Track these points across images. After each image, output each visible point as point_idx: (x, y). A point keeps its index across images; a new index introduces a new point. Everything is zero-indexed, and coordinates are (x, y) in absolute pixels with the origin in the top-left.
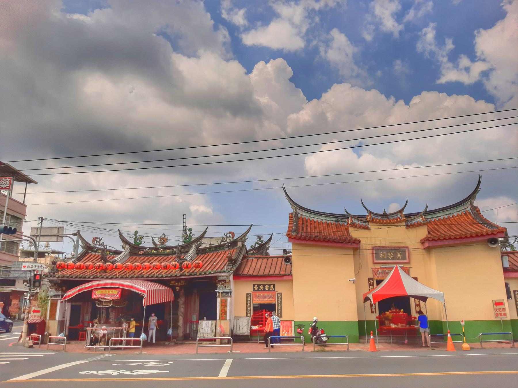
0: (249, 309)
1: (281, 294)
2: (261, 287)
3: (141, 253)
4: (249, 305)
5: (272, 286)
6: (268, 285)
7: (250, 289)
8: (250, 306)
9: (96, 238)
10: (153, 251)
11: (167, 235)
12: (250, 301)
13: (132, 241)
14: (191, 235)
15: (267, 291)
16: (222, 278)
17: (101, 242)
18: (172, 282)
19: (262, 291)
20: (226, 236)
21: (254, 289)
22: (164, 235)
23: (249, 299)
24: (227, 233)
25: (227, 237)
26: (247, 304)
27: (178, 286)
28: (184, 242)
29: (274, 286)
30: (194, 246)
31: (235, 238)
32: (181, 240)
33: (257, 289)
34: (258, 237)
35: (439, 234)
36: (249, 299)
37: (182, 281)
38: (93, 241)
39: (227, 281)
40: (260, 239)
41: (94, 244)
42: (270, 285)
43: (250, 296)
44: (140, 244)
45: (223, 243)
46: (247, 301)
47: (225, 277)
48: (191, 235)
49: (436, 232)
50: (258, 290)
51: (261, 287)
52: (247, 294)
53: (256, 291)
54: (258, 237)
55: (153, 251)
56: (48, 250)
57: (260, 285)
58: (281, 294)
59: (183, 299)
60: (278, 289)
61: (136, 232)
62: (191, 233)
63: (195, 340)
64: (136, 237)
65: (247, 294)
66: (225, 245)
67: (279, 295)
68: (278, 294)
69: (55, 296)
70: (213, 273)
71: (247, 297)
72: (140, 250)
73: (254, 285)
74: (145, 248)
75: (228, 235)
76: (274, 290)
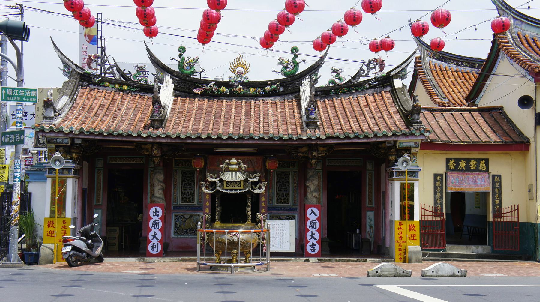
0: (439, 202)
1: (500, 176)
2: (463, 164)
4: (439, 194)
5: (482, 164)
6: (476, 160)
7: (441, 169)
8: (442, 197)
10: (223, 89)
11: (247, 59)
12: (441, 187)
13: (174, 66)
14: (298, 60)
15: (473, 170)
18: (305, 149)
19: (463, 170)
20: (368, 66)
21: (448, 167)
22: (241, 57)
23: (438, 184)
24: (370, 62)
25: (369, 68)
28: (284, 74)
29: (487, 161)
30: (307, 82)
31: (386, 70)
32: (280, 68)
33: (455, 166)
34: (335, 71)
36: (438, 184)
37: (321, 149)
39: (413, 151)
40: (338, 74)
42: (478, 161)
43: (441, 179)
45: (361, 79)
46: (435, 188)
47: (412, 144)
48: (298, 60)
50: (457, 169)
51: (463, 164)
52: (436, 175)
53: (453, 170)
54: (335, 71)
55: (223, 89)
57: (460, 160)
58: (500, 176)
59: (161, 177)
60: (494, 169)
61: (182, 50)
63: (265, 255)
65: (436, 175)
66: (366, 82)
67: (497, 179)
68: (494, 176)
69: (62, 171)
71: (435, 181)
72: (196, 87)
73: (448, 161)
74: (207, 82)
75: (372, 65)
76: (487, 170)
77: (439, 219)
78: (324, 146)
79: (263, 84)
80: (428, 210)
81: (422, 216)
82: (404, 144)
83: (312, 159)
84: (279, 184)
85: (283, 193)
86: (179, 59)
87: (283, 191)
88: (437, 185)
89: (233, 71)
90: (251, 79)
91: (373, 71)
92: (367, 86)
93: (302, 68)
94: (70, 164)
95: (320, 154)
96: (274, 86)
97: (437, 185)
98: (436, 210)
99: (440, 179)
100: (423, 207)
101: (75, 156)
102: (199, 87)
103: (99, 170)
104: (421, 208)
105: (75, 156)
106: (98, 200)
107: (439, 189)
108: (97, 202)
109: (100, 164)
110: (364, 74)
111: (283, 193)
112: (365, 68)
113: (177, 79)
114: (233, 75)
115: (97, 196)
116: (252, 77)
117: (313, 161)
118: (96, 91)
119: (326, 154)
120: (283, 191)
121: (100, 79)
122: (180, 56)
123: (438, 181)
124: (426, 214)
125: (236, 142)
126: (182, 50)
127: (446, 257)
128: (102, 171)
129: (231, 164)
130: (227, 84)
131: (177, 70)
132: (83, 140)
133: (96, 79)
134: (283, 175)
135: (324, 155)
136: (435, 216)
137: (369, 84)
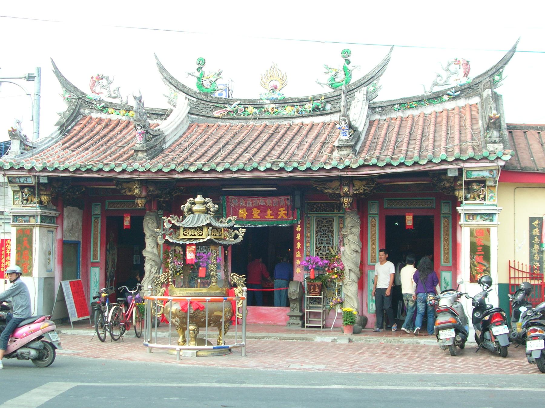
3: (216, 113)
9: (100, 78)
13: (192, 84)
14: (350, 67)
16: (475, 175)
17: (113, 87)
18: (336, 184)
23: (536, 232)
26: (532, 245)
27: (346, 195)
30: (360, 95)
35: (194, 242)
36: (536, 232)
37: (357, 184)
38: (92, 86)
39: (488, 184)
41: (93, 92)
44: (214, 91)
46: (532, 237)
47: (486, 174)
49: (81, 134)
52: (532, 220)
55: (251, 109)
56: (116, 101)
61: (201, 63)
62: (349, 62)
64: (203, 75)
65: (532, 220)
70: (438, 164)
71: (532, 227)
77: (536, 282)
78: (361, 179)
79: (302, 101)
80: (520, 269)
81: (510, 278)
82: (474, 173)
83: (344, 197)
84: (319, 234)
85: (324, 247)
86: (198, 74)
87: (325, 244)
88: (534, 233)
89: (263, 85)
90: (287, 96)
91: (454, 77)
92: (446, 98)
93: (356, 77)
94: (36, 209)
95: (356, 190)
96: (316, 103)
97: (534, 233)
98: (532, 268)
99: (538, 224)
100: (512, 265)
101: (44, 198)
102: (221, 108)
103: (96, 218)
104: (510, 267)
105: (44, 198)
106: (95, 257)
107: (536, 239)
108: (94, 259)
109: (97, 210)
110: (442, 82)
111: (324, 247)
112: (444, 75)
113: (195, 99)
114: (264, 91)
115: (94, 251)
116: (291, 92)
117: (346, 200)
118: (151, 128)
119: (365, 190)
120: (325, 244)
121: (103, 104)
122: (199, 69)
123: (535, 228)
124: (517, 276)
125: (236, 176)
126: (201, 63)
127: (68, 354)
128: (99, 219)
129: (194, 203)
130: (257, 104)
131: (195, 89)
132: (49, 178)
133: (98, 105)
134: (325, 222)
135: (361, 191)
136: (531, 278)
137: (449, 95)
